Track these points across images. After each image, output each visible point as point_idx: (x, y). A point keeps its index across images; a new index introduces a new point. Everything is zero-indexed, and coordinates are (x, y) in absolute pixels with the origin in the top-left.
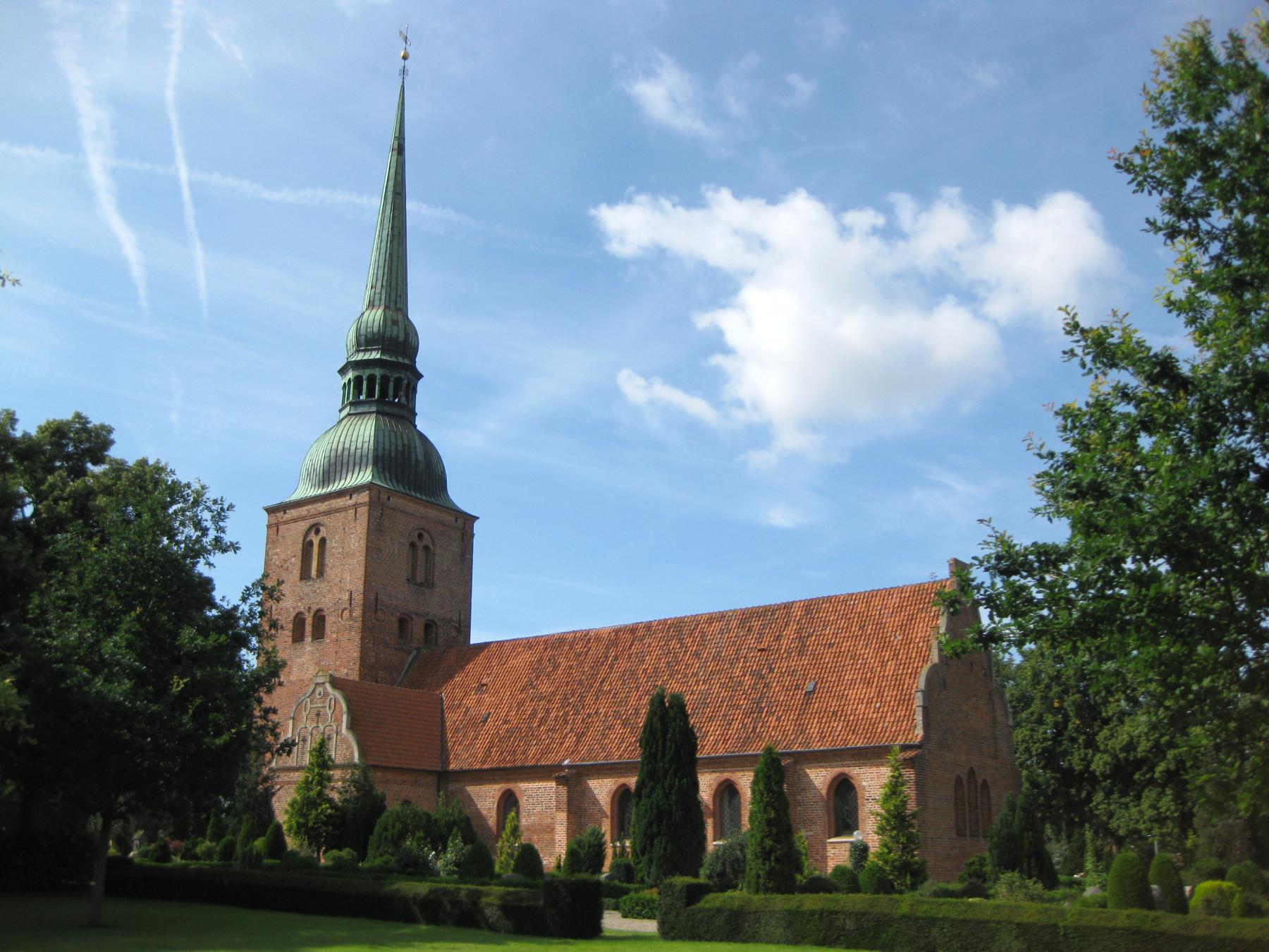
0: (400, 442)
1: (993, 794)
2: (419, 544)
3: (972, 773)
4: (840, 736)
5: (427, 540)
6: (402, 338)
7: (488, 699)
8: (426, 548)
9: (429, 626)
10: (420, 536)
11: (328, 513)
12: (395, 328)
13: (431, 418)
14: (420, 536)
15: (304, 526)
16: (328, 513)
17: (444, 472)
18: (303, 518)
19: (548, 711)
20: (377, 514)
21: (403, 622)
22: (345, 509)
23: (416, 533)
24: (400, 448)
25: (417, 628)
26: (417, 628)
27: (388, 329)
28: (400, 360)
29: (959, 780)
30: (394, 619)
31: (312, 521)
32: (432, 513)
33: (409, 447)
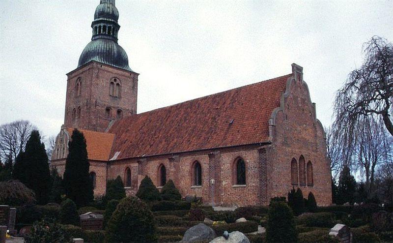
0: (108, 48)
1: (314, 167)
2: (115, 83)
3: (302, 158)
4: (239, 140)
5: (118, 81)
6: (111, 12)
7: (128, 134)
8: (118, 84)
9: (119, 112)
10: (115, 80)
11: (82, 73)
12: (108, 9)
13: (124, 39)
14: (115, 80)
15: (76, 78)
16: (82, 73)
17: (127, 58)
18: (75, 76)
19: (144, 137)
20: (319, 133)
21: (108, 110)
22: (86, 70)
23: (113, 79)
24: (108, 49)
25: (114, 112)
26: (114, 112)
27: (106, 10)
28: (110, 20)
29: (294, 161)
30: (104, 109)
31: (78, 77)
32: (120, 72)
33: (111, 49)
